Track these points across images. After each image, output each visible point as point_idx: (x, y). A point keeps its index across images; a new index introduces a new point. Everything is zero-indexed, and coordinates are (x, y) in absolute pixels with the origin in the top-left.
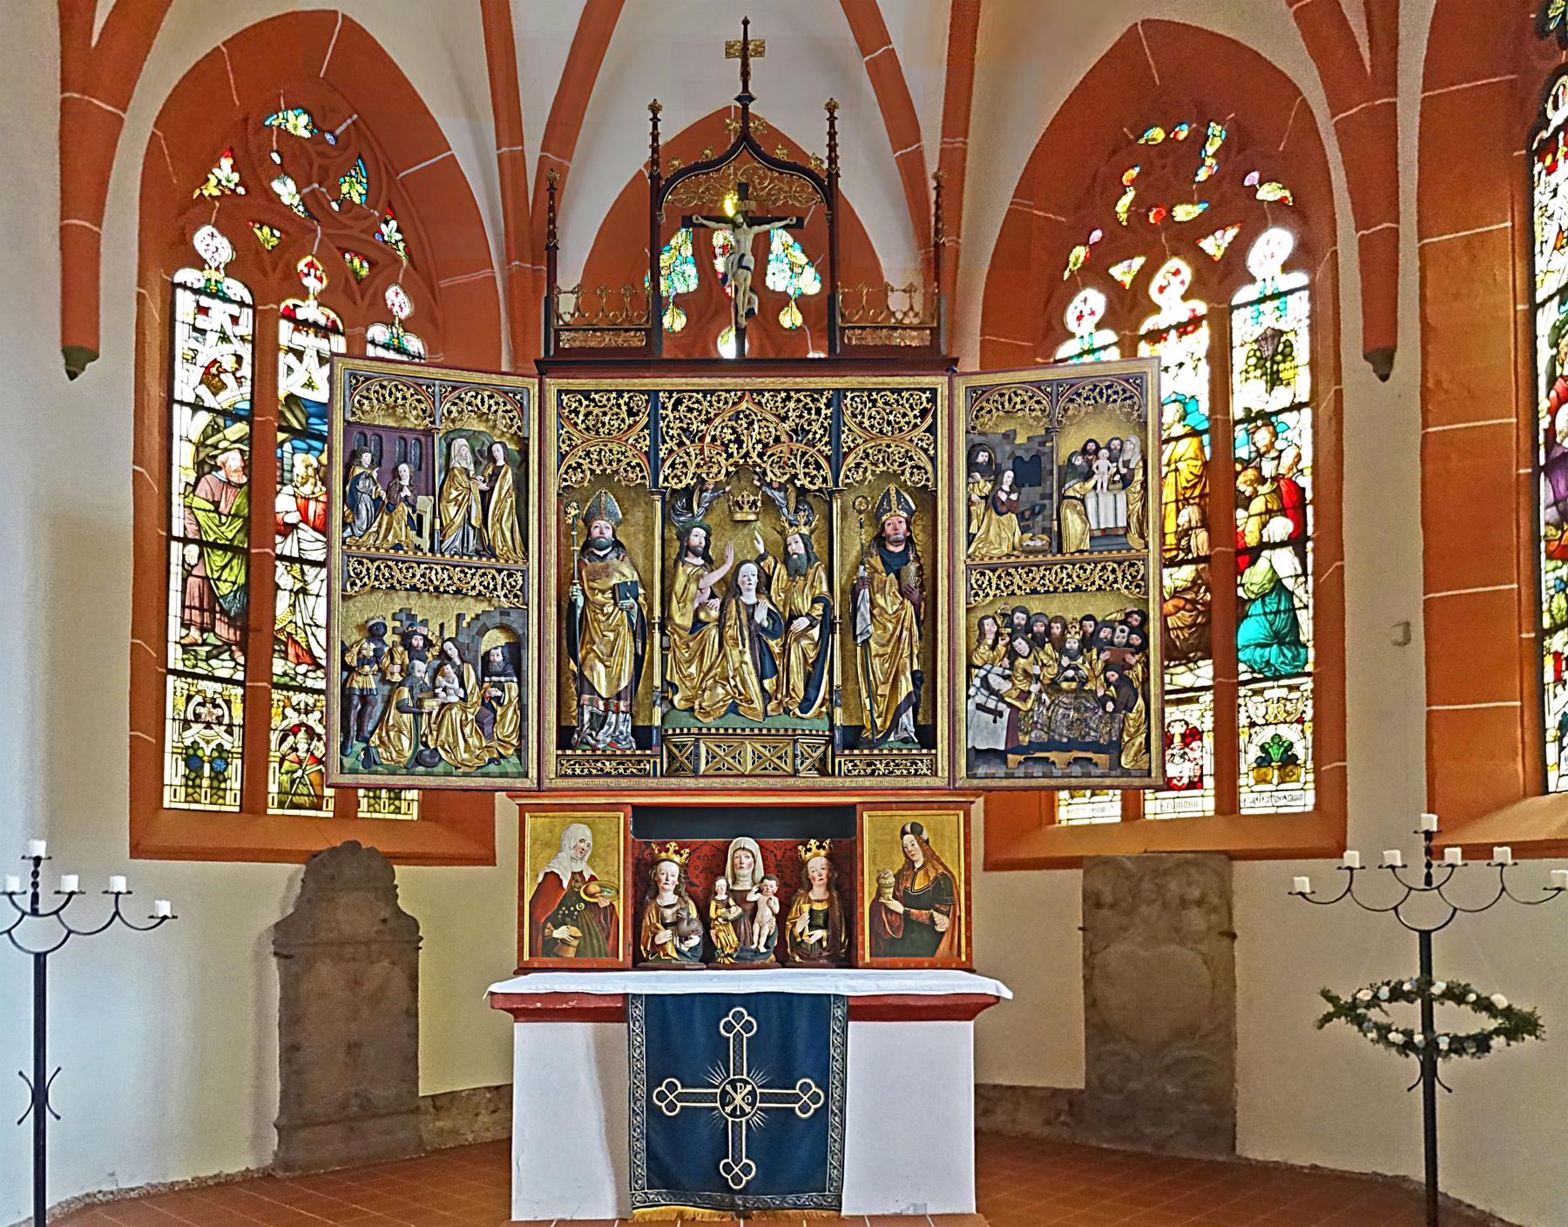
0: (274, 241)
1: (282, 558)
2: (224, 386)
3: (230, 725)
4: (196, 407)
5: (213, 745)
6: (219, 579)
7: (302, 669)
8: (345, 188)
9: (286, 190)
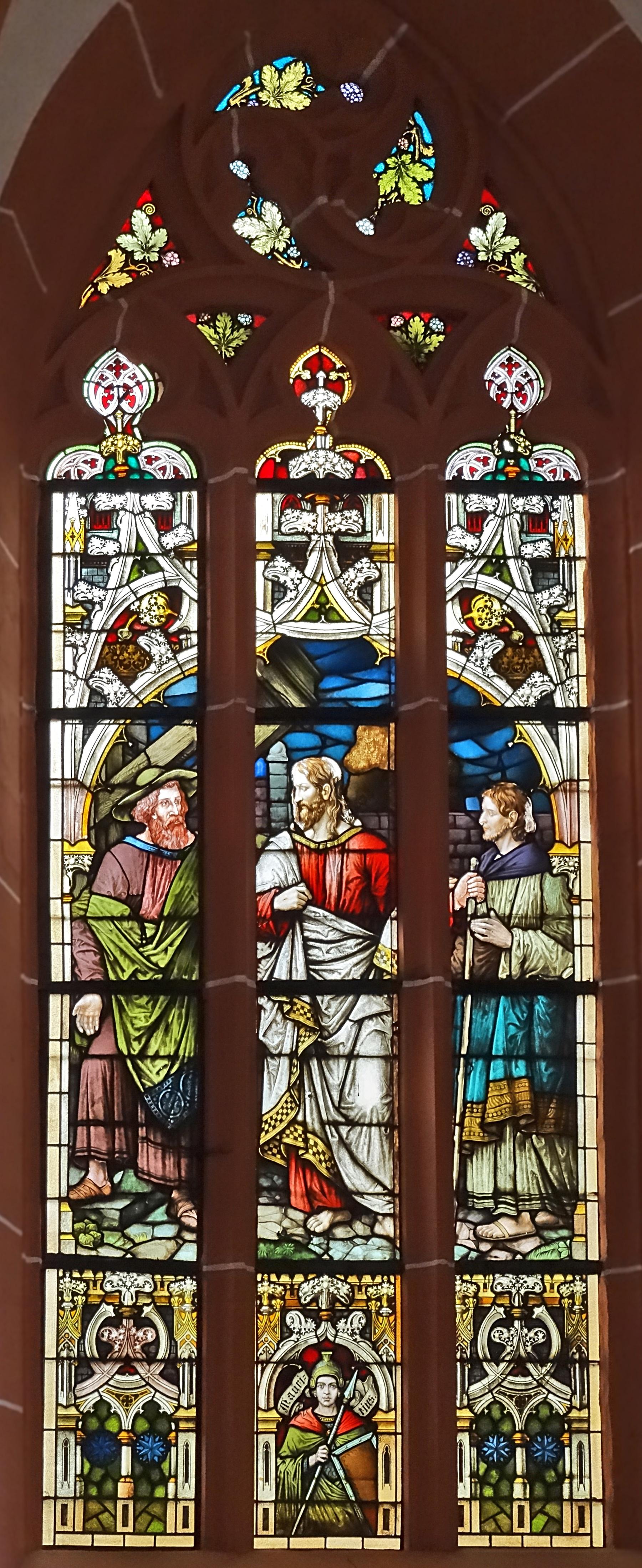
0: (241, 337)
1: (272, 987)
2: (146, 658)
3: (172, 1361)
4: (90, 716)
5: (137, 1407)
6: (142, 1055)
7: (323, 1221)
8: (386, 184)
9: (262, 229)
